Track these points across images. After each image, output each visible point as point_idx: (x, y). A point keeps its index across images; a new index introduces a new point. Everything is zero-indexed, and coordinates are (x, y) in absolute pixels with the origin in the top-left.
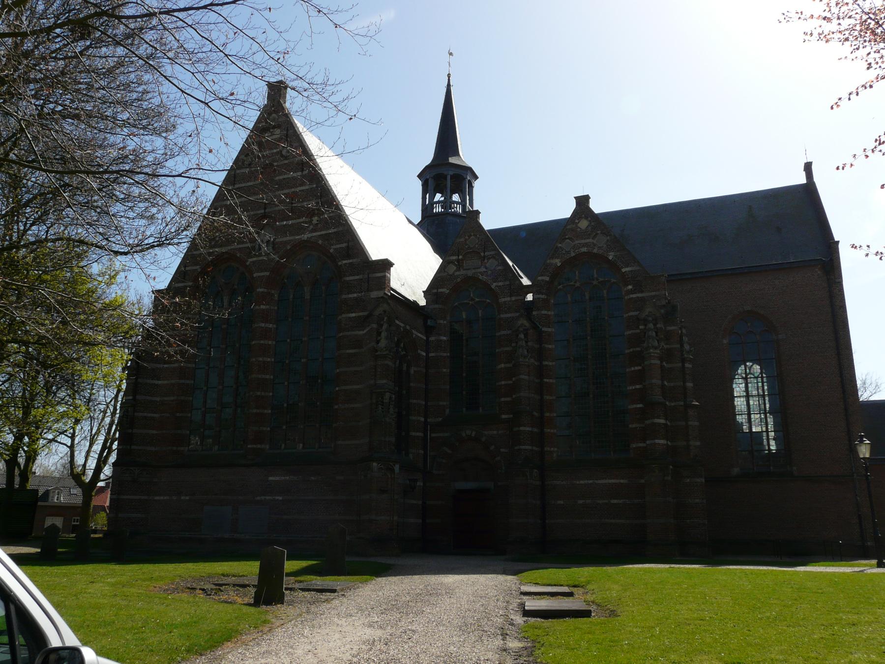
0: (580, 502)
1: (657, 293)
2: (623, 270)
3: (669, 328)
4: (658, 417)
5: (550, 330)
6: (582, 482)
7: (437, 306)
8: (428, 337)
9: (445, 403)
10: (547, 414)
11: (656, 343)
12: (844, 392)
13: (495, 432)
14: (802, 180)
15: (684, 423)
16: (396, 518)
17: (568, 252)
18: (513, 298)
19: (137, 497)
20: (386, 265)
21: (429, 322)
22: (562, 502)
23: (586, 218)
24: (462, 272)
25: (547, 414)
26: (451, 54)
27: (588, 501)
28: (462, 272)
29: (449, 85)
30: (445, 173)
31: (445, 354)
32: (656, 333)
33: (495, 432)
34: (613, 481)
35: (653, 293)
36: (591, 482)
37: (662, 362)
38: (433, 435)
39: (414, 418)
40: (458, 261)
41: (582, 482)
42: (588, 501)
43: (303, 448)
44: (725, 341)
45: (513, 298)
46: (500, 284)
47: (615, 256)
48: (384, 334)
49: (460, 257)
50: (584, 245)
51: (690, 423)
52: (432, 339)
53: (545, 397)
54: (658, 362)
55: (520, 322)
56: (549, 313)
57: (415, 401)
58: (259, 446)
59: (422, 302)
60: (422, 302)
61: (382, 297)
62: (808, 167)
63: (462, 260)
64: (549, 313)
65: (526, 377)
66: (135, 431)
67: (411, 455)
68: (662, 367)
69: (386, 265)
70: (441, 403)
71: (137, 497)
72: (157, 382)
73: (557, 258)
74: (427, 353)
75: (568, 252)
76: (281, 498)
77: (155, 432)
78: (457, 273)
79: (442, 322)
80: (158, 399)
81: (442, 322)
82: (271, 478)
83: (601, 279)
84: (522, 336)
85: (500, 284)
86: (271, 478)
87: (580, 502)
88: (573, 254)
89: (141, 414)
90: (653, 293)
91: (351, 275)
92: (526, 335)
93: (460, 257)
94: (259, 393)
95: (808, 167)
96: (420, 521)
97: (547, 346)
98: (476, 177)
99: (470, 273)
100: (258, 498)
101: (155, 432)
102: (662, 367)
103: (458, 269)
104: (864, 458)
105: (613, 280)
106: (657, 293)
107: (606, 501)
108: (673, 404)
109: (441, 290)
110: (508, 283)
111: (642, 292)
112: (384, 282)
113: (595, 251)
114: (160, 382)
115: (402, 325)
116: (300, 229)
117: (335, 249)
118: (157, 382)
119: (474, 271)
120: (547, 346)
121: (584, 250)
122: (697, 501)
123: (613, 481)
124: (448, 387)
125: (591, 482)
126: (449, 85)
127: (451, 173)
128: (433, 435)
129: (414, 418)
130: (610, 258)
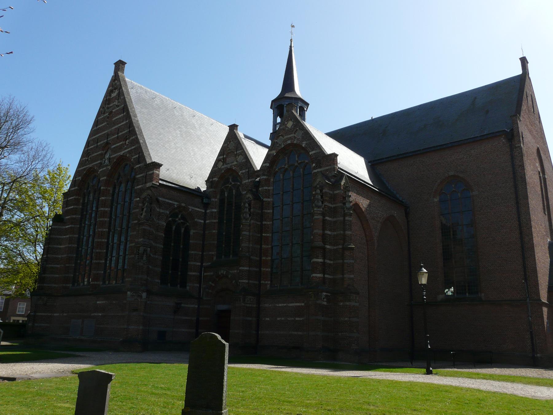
0: (279, 319)
1: (329, 167)
2: (310, 153)
3: (336, 192)
4: (317, 258)
5: (269, 200)
6: (280, 305)
7: (211, 190)
8: (206, 210)
9: (213, 253)
10: (264, 258)
11: (320, 204)
12: (521, 233)
13: (236, 271)
14: (519, 71)
15: (341, 261)
16: (141, 327)
17: (280, 145)
18: (250, 180)
19: (46, 314)
20: (157, 166)
21: (205, 201)
22: (268, 319)
23: (291, 120)
24: (225, 166)
25: (264, 258)
26: (293, 26)
27: (283, 319)
28: (225, 166)
29: (291, 47)
30: (283, 104)
31: (215, 221)
32: (322, 197)
33: (236, 271)
34: (298, 304)
35: (327, 168)
36: (285, 305)
37: (324, 217)
38: (205, 274)
39: (192, 263)
40: (223, 158)
41: (280, 305)
42: (283, 319)
43: (116, 283)
44: (436, 200)
45: (250, 180)
46: (244, 171)
47: (306, 144)
48: (145, 209)
49: (225, 156)
50: (290, 139)
51: (345, 261)
52: (208, 211)
53: (263, 246)
54: (321, 217)
55: (248, 196)
56: (269, 188)
57: (192, 252)
58: (96, 283)
59: (203, 188)
60: (203, 188)
61: (152, 186)
62: (524, 61)
63: (226, 158)
64: (269, 188)
65: (247, 233)
66: (46, 275)
67: (188, 288)
68: (324, 221)
69: (157, 166)
70: (210, 253)
71: (46, 314)
72: (59, 246)
73: (274, 150)
74: (205, 221)
75: (280, 145)
76: (100, 314)
77: (57, 276)
78: (223, 167)
79: (214, 200)
80: (60, 256)
81: (214, 200)
82: (98, 302)
83: (299, 162)
84: (247, 205)
85: (244, 171)
86: (98, 302)
87: (279, 319)
88: (283, 146)
89: (50, 265)
90: (327, 168)
91: (139, 174)
92: (250, 205)
93: (225, 156)
94: (97, 251)
95: (524, 61)
96: (194, 330)
97: (266, 211)
98: (307, 104)
99: (228, 166)
100: (92, 315)
101: (57, 276)
102: (324, 221)
103: (223, 165)
104: (422, 284)
105: (306, 161)
106: (329, 167)
107: (293, 319)
108: (335, 248)
109: (214, 179)
110: (247, 170)
111: (320, 167)
112: (151, 177)
113: (295, 142)
114: (62, 246)
115: (176, 203)
116: (120, 148)
117: (134, 159)
118: (59, 246)
119: (231, 164)
120: (266, 211)
121: (289, 142)
122: (346, 319)
123: (298, 304)
124: (216, 242)
125: (285, 305)
126: (291, 47)
127: (287, 103)
128: (205, 274)
129: (192, 263)
130: (303, 146)
